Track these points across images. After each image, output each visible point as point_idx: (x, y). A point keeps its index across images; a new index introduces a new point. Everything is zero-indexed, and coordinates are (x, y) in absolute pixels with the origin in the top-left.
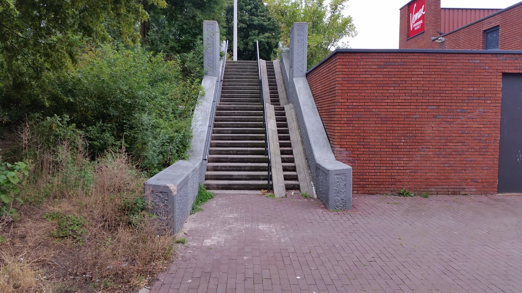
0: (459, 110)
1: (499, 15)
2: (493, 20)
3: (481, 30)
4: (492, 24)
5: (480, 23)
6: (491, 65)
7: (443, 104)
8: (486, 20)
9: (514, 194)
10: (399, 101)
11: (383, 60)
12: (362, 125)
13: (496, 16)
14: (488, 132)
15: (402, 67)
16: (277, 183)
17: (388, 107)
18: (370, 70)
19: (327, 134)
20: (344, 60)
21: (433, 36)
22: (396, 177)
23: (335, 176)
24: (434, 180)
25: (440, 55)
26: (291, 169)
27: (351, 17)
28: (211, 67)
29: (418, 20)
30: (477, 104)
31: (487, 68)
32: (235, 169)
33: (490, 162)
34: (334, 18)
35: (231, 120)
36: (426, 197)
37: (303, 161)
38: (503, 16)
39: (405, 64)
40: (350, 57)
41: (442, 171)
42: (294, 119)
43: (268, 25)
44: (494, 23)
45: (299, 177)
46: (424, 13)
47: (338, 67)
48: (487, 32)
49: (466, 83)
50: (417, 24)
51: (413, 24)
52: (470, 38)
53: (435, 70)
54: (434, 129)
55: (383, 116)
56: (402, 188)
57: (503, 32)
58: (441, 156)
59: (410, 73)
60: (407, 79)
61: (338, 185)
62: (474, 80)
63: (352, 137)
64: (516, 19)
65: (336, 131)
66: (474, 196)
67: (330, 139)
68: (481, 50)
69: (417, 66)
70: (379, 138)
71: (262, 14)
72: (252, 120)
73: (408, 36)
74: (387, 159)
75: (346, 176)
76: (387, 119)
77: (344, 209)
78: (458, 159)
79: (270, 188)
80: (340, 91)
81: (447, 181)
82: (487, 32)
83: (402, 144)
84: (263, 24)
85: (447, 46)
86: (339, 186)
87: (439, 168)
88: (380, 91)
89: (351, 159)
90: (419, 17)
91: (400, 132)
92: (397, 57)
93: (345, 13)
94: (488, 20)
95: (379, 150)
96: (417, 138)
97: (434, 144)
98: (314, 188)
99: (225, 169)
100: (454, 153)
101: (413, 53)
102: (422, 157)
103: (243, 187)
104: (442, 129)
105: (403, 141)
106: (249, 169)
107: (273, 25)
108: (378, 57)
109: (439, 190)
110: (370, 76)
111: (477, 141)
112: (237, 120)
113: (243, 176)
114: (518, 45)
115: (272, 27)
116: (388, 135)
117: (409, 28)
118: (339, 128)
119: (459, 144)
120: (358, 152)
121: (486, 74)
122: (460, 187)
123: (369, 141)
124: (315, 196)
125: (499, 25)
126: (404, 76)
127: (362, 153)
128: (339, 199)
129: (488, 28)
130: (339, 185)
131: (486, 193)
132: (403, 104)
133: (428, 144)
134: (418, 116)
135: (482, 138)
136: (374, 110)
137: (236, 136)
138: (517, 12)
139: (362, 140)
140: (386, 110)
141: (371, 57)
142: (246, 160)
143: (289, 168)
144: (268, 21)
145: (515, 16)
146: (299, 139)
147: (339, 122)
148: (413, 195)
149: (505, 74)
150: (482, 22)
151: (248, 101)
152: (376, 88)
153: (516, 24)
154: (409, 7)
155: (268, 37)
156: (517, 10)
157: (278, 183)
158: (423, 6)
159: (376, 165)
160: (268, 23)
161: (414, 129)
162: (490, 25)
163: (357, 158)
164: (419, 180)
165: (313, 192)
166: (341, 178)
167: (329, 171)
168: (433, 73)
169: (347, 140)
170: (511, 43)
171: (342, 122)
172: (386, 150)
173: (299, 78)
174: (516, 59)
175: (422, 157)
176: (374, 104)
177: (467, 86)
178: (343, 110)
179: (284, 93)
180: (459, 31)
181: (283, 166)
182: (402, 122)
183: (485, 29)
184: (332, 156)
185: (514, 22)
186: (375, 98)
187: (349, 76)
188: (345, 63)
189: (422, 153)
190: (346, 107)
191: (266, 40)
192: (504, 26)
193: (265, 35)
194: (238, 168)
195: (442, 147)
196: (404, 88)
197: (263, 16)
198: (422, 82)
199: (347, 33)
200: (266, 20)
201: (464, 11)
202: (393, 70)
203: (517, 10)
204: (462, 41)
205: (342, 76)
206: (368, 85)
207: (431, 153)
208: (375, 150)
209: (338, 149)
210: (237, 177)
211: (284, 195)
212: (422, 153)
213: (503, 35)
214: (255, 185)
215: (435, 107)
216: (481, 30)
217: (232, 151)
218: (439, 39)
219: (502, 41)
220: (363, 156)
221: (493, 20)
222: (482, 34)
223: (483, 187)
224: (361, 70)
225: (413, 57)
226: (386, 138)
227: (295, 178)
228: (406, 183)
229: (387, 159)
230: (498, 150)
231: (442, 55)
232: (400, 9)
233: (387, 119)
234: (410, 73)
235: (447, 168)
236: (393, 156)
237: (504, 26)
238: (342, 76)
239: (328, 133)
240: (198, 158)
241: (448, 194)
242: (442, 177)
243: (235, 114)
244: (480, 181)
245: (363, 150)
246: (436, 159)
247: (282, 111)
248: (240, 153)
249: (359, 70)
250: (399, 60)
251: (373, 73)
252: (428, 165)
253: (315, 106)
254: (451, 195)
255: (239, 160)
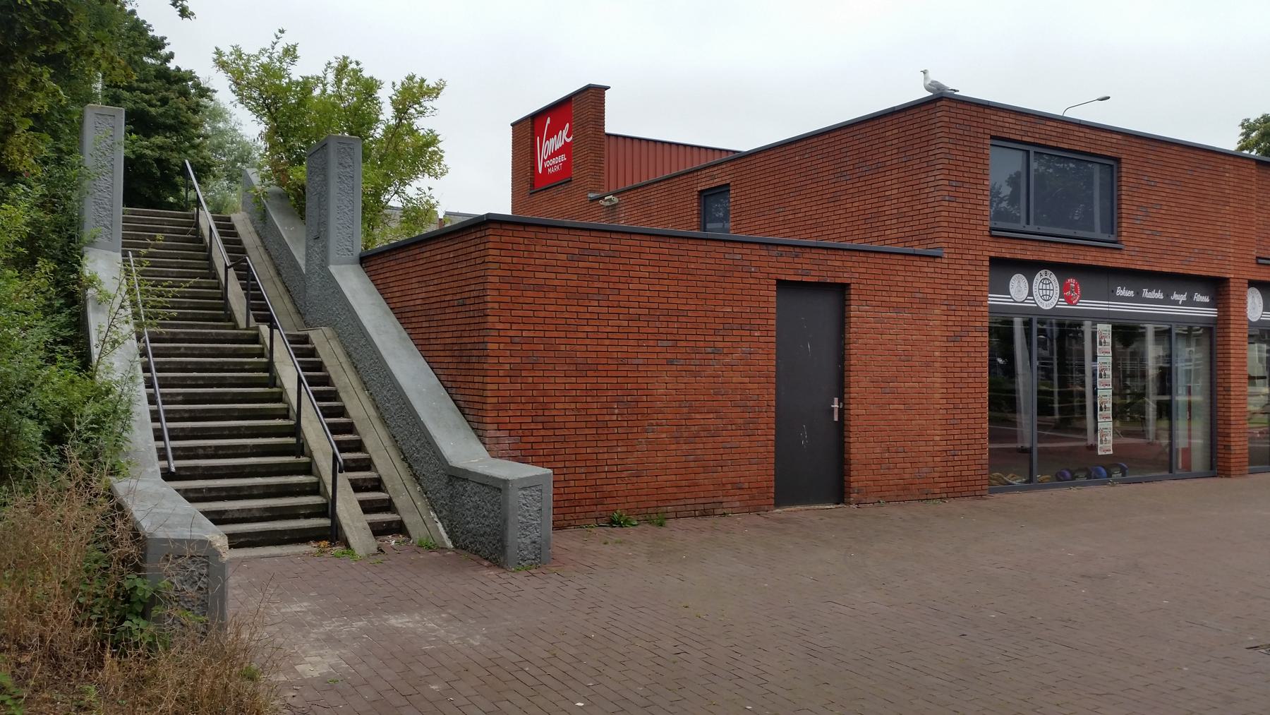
0: (709, 350)
1: (729, 165)
2: (718, 172)
3: (695, 189)
4: (715, 181)
5: (691, 175)
6: (759, 264)
7: (683, 337)
8: (703, 172)
9: (799, 507)
10: (609, 329)
11: (579, 245)
12: (540, 380)
13: (724, 166)
14: (757, 392)
15: (612, 260)
16: (350, 522)
17: (588, 342)
18: (554, 262)
19: (454, 401)
20: (503, 239)
21: (591, 191)
22: (605, 488)
23: (520, 493)
24: (670, 490)
25: (677, 240)
26: (369, 486)
27: (436, 133)
28: (105, 226)
29: (555, 154)
30: (738, 339)
31: (753, 269)
32: (224, 494)
33: (762, 450)
34: (394, 133)
35: (172, 366)
36: (661, 525)
37: (397, 465)
38: (736, 167)
39: (617, 254)
40: (516, 234)
41: (683, 471)
42: (346, 366)
43: (161, 115)
44: (720, 179)
45: (398, 502)
46: (568, 140)
47: (491, 252)
48: (706, 194)
49: (721, 297)
50: (554, 161)
51: (544, 161)
52: (674, 202)
53: (668, 270)
54: (669, 386)
55: (580, 361)
56: (615, 511)
57: (738, 198)
58: (682, 440)
59: (626, 274)
60: (621, 286)
61: (525, 512)
62: (733, 291)
63: (521, 407)
64: (762, 176)
65: (489, 393)
66: (739, 517)
67: (467, 411)
68: (696, 231)
69: (639, 261)
70: (573, 406)
71: (144, 85)
72: (231, 367)
73: (533, 185)
74: (589, 450)
75: (541, 490)
76: (587, 367)
77: (536, 564)
78: (709, 446)
79: (334, 535)
80: (496, 306)
81: (692, 489)
82: (706, 194)
83: (614, 418)
84: (148, 112)
85: (623, 215)
86: (527, 514)
87: (679, 465)
88: (574, 309)
89: (518, 453)
90: (557, 147)
91: (610, 393)
92: (603, 240)
93: (423, 124)
94: (707, 171)
95: (573, 432)
96: (640, 405)
97: (670, 416)
98: (440, 525)
99: (196, 495)
100: (702, 434)
101: (631, 233)
102: (650, 443)
103: (261, 538)
104: (683, 386)
105: (616, 411)
106: (262, 492)
107: (175, 117)
108: (568, 237)
109: (679, 508)
110: (553, 276)
111: (739, 410)
112: (189, 367)
113: (254, 512)
114: (767, 226)
115: (172, 122)
116: (589, 399)
117: (535, 167)
118: (495, 387)
119: (711, 416)
120: (532, 439)
121: (752, 281)
122: (715, 500)
123: (554, 413)
124: (449, 544)
125: (729, 184)
126: (616, 279)
127: (540, 439)
128: (528, 541)
129: (708, 187)
130: (528, 511)
131: (757, 510)
132: (615, 336)
133: (660, 416)
134: (641, 361)
135: (748, 403)
136: (563, 347)
137: (203, 410)
138: (763, 163)
139: (540, 412)
140: (584, 348)
141: (555, 236)
142: (247, 470)
143: (365, 484)
144: (161, 106)
145: (758, 169)
146: (372, 412)
147: (495, 373)
148: (636, 523)
149: (781, 284)
150: (695, 174)
151: (189, 316)
152: (566, 302)
153: (762, 185)
154: (533, 123)
155: (161, 148)
156: (762, 160)
157: (353, 522)
158: (568, 125)
159: (567, 464)
160: (161, 110)
161: (635, 386)
162: (711, 182)
163: (531, 452)
164: (644, 492)
165: (441, 536)
166: (531, 496)
167: (506, 481)
168: (666, 276)
169: (510, 413)
170: (752, 220)
171: (501, 373)
172: (587, 431)
173: (343, 266)
174: (797, 256)
175: (650, 443)
176: (563, 334)
177: (721, 303)
178: (502, 346)
179: (287, 300)
180: (649, 187)
181: (350, 480)
182: (614, 374)
183: (703, 188)
184: (480, 448)
185: (757, 182)
186: (563, 321)
187: (515, 274)
188: (504, 246)
189: (650, 435)
190: (508, 340)
191: (157, 154)
192: (739, 186)
193: (153, 140)
194: (233, 493)
195: (683, 422)
196: (615, 304)
197: (146, 92)
198: (648, 293)
199: (427, 168)
200: (154, 102)
201: (636, 143)
202: (596, 265)
203: (762, 160)
204: (656, 207)
205: (500, 273)
206: (551, 295)
207: (664, 435)
208: (566, 432)
209: (492, 433)
210: (237, 515)
211: (374, 549)
212: (650, 435)
213: (738, 203)
214: (293, 531)
215: (670, 343)
216: (695, 189)
217: (204, 448)
218: (606, 198)
219: (736, 215)
220: (543, 446)
221: (718, 172)
222: (696, 197)
223: (753, 498)
224: (538, 262)
225: (630, 242)
226: (585, 406)
227: (388, 506)
228: (623, 500)
229: (589, 450)
230: (774, 426)
231: (681, 241)
232: (513, 125)
233: (587, 367)
234: (626, 274)
235: (692, 464)
236: (600, 444)
237: (739, 186)
238: (500, 273)
239: (459, 397)
240: (150, 470)
241: (695, 516)
242: (684, 483)
243: (178, 352)
244: (746, 485)
245: (542, 432)
246: (673, 447)
247: (304, 346)
248: (224, 452)
249: (532, 261)
250: (607, 247)
251: (561, 270)
252: (660, 459)
253: (405, 334)
254: (700, 518)
255: (228, 472)
